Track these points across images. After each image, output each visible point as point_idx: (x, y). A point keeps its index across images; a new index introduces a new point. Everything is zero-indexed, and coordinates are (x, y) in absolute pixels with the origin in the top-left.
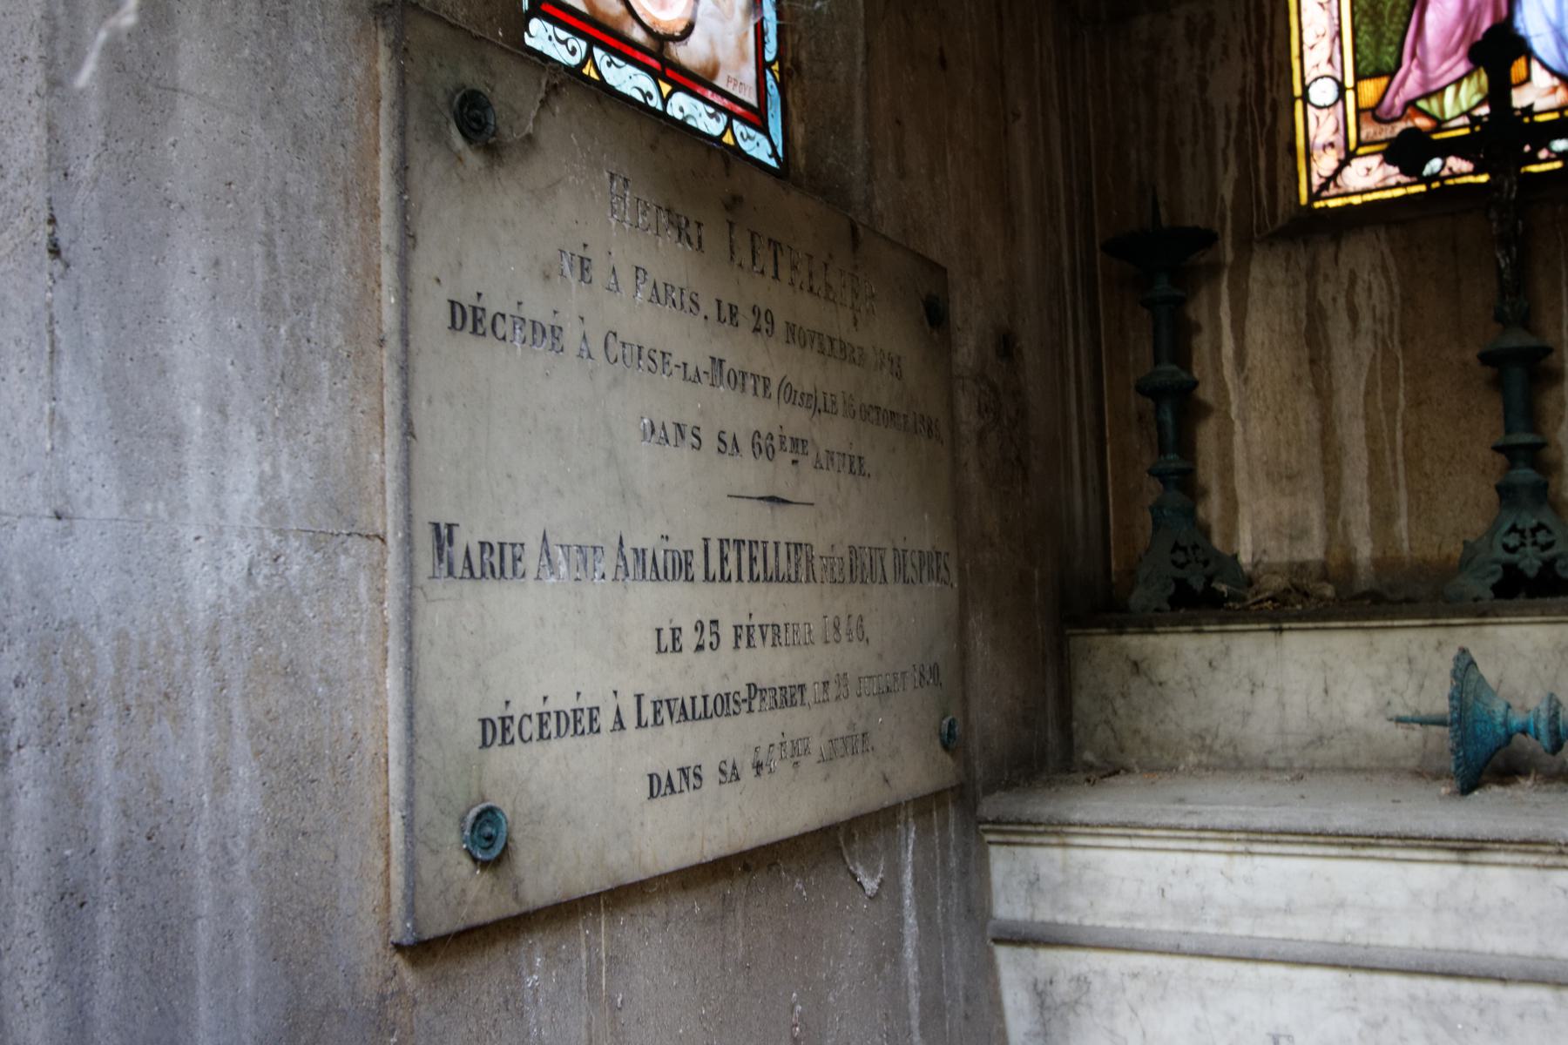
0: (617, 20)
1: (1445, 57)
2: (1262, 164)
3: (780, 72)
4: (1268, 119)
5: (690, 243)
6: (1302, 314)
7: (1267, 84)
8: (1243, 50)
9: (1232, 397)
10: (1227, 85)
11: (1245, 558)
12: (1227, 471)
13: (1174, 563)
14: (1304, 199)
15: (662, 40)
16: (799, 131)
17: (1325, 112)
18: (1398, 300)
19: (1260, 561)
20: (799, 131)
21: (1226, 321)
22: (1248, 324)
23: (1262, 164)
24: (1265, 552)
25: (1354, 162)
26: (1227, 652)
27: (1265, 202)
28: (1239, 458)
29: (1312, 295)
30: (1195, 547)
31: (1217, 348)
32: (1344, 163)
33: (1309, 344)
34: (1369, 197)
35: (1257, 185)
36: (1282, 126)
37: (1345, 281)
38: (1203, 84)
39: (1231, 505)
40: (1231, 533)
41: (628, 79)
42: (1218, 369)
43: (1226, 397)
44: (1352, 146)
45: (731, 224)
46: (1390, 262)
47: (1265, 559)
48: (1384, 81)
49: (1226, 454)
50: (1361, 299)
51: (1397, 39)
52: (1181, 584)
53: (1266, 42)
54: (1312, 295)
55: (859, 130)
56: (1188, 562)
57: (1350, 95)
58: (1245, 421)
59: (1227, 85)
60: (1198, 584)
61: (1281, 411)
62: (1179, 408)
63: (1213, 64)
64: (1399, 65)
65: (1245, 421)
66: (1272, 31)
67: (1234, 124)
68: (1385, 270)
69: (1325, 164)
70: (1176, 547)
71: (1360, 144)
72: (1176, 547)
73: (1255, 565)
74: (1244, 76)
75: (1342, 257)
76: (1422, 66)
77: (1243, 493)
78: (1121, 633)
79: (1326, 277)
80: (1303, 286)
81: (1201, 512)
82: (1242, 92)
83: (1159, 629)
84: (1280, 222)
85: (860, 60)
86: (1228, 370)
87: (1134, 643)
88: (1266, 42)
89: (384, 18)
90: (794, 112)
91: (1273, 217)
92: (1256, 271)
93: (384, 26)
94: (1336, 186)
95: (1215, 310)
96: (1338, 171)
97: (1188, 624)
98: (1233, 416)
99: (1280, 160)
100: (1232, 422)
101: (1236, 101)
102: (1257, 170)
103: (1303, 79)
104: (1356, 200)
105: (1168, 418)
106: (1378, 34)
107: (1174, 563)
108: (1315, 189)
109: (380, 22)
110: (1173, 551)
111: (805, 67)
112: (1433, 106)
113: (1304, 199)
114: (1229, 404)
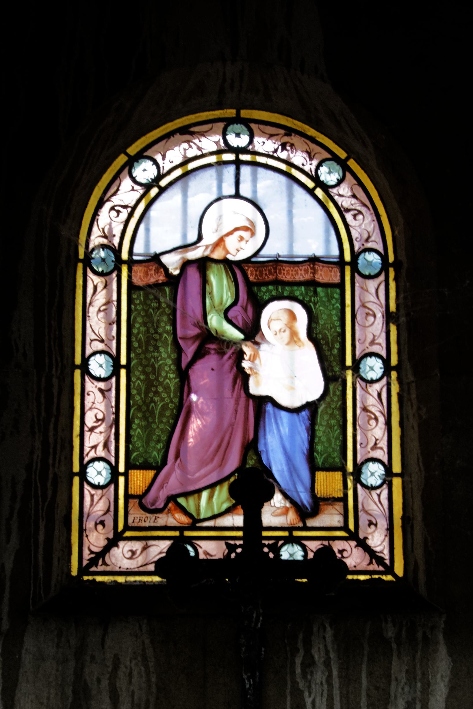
1: (203, 463)
2: (41, 537)
4: (50, 493)
6: (69, 691)
14: (74, 572)
18: (154, 690)
22: (18, 695)
23: (41, 537)
25: (121, 544)
29: (79, 674)
32: (112, 543)
34: (131, 579)
37: (109, 663)
44: (121, 527)
46: (150, 652)
48: (151, 474)
50: (122, 683)
51: (164, 438)
54: (79, 674)
57: (122, 480)
64: (164, 462)
68: (145, 658)
69: (96, 540)
71: (127, 527)
75: (108, 642)
76: (184, 469)
79: (93, 657)
80: (72, 664)
94: (105, 563)
96: (107, 549)
103: (82, 458)
104: (121, 579)
106: (147, 428)
112: (189, 504)
113: (74, 572)
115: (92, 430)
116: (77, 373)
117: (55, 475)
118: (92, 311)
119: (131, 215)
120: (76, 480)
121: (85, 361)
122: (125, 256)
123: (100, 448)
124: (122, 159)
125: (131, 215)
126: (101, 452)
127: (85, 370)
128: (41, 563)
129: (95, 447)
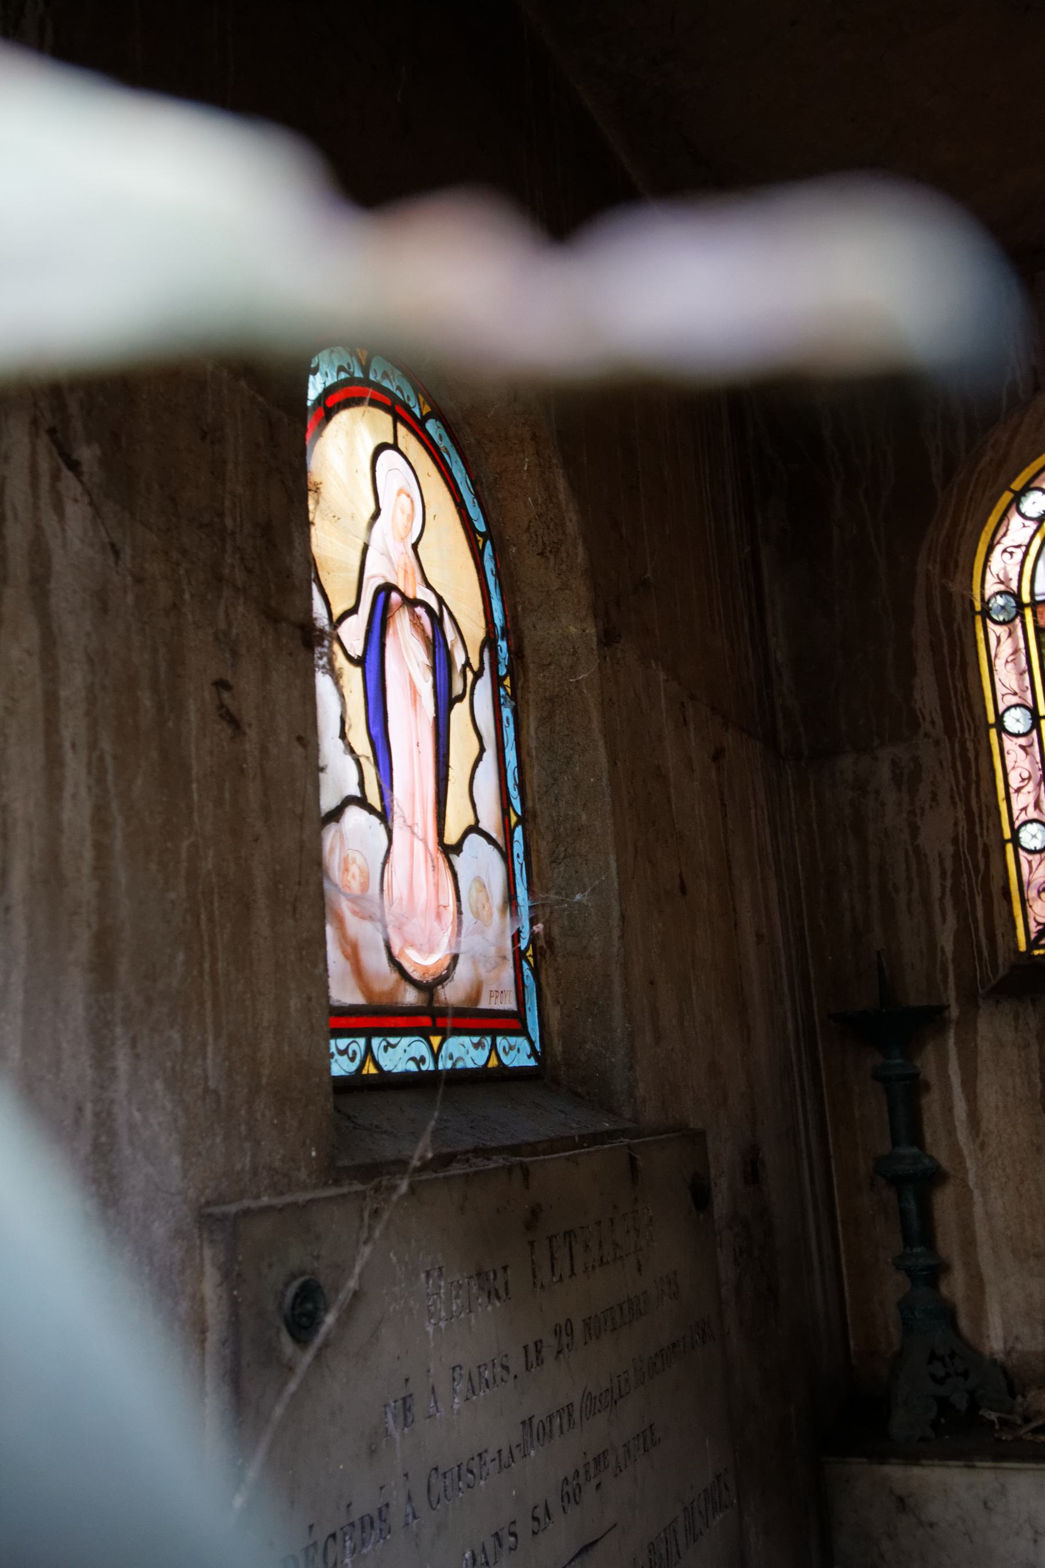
0: (393, 992)
2: (980, 914)
3: (534, 956)
4: (982, 867)
5: (499, 1298)
7: (978, 831)
8: (952, 798)
9: (969, 1164)
10: (938, 833)
11: (995, 1343)
12: (969, 1244)
13: (933, 1377)
14: (1023, 947)
15: (429, 988)
16: (554, 1014)
17: (1037, 857)
19: (1013, 1349)
20: (554, 1014)
21: (956, 1080)
23: (980, 914)
24: (1017, 1338)
26: (1003, 1491)
27: (986, 954)
28: (981, 1232)
30: (953, 1355)
31: (948, 1109)
33: (918, 846)
35: (977, 936)
36: (995, 870)
38: (914, 831)
39: (977, 1284)
40: (979, 1317)
41: (400, 1055)
42: (951, 1131)
43: (962, 1162)
45: (531, 1243)
47: (1019, 1347)
49: (966, 1225)
52: (944, 1404)
53: (974, 786)
55: (617, 1010)
56: (948, 1375)
58: (985, 1192)
59: (938, 833)
60: (960, 1401)
61: (1022, 1183)
62: (919, 1183)
63: (923, 809)
65: (985, 1192)
66: (978, 775)
67: (949, 874)
70: (933, 1357)
72: (933, 1357)
73: (1008, 1353)
74: (956, 824)
77: (988, 1271)
78: (882, 1463)
81: (944, 1289)
82: (955, 841)
83: (924, 1462)
84: (1002, 972)
85: (616, 933)
86: (962, 1135)
87: (896, 1472)
88: (974, 786)
89: (211, 1232)
90: (548, 994)
91: (995, 968)
92: (983, 1026)
93: (212, 1242)
95: (942, 1063)
97: (958, 1460)
98: (971, 1184)
99: (996, 907)
100: (971, 1191)
101: (950, 849)
102: (975, 921)
103: (1012, 823)
105: (912, 1205)
107: (933, 1377)
108: (1033, 936)
109: (205, 1235)
110: (930, 1362)
111: (558, 943)
113: (1023, 947)
114: (965, 1171)
115: (1018, 790)
116: (993, 733)
117: (985, 845)
118: (999, 664)
119: (1026, 554)
120: (1009, 847)
121: (999, 718)
122: (1026, 598)
123: (1031, 809)
124: (1007, 497)
125: (1026, 554)
126: (1032, 814)
127: (1001, 728)
128: (984, 941)
129: (1025, 809)
